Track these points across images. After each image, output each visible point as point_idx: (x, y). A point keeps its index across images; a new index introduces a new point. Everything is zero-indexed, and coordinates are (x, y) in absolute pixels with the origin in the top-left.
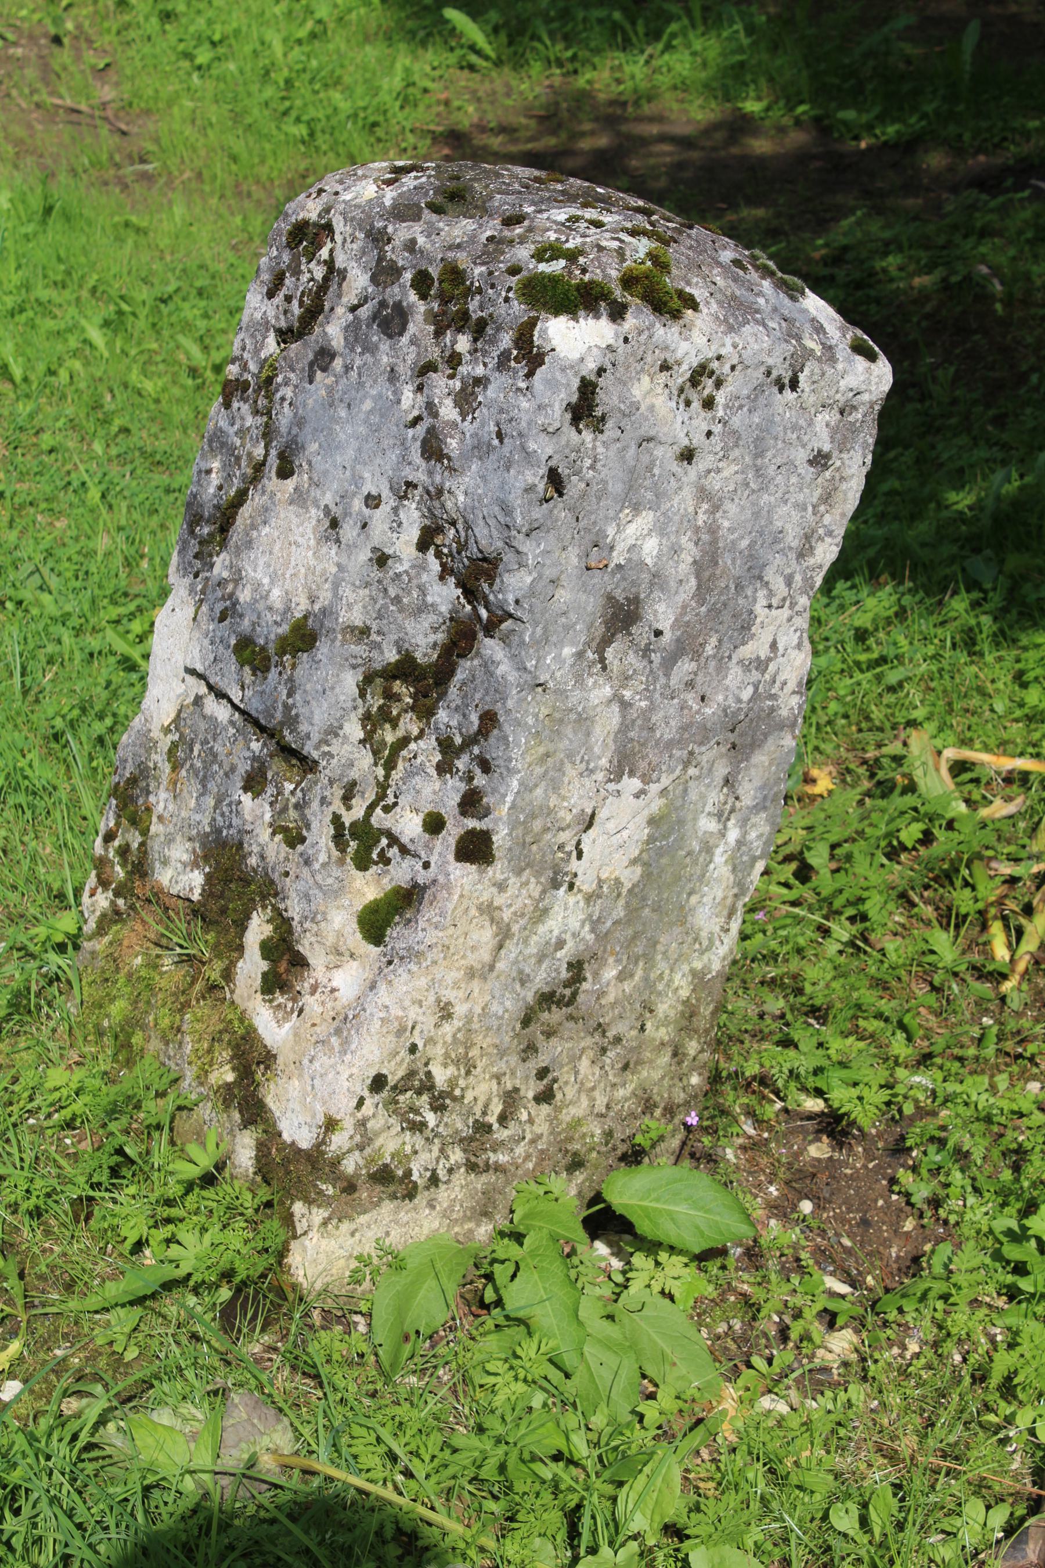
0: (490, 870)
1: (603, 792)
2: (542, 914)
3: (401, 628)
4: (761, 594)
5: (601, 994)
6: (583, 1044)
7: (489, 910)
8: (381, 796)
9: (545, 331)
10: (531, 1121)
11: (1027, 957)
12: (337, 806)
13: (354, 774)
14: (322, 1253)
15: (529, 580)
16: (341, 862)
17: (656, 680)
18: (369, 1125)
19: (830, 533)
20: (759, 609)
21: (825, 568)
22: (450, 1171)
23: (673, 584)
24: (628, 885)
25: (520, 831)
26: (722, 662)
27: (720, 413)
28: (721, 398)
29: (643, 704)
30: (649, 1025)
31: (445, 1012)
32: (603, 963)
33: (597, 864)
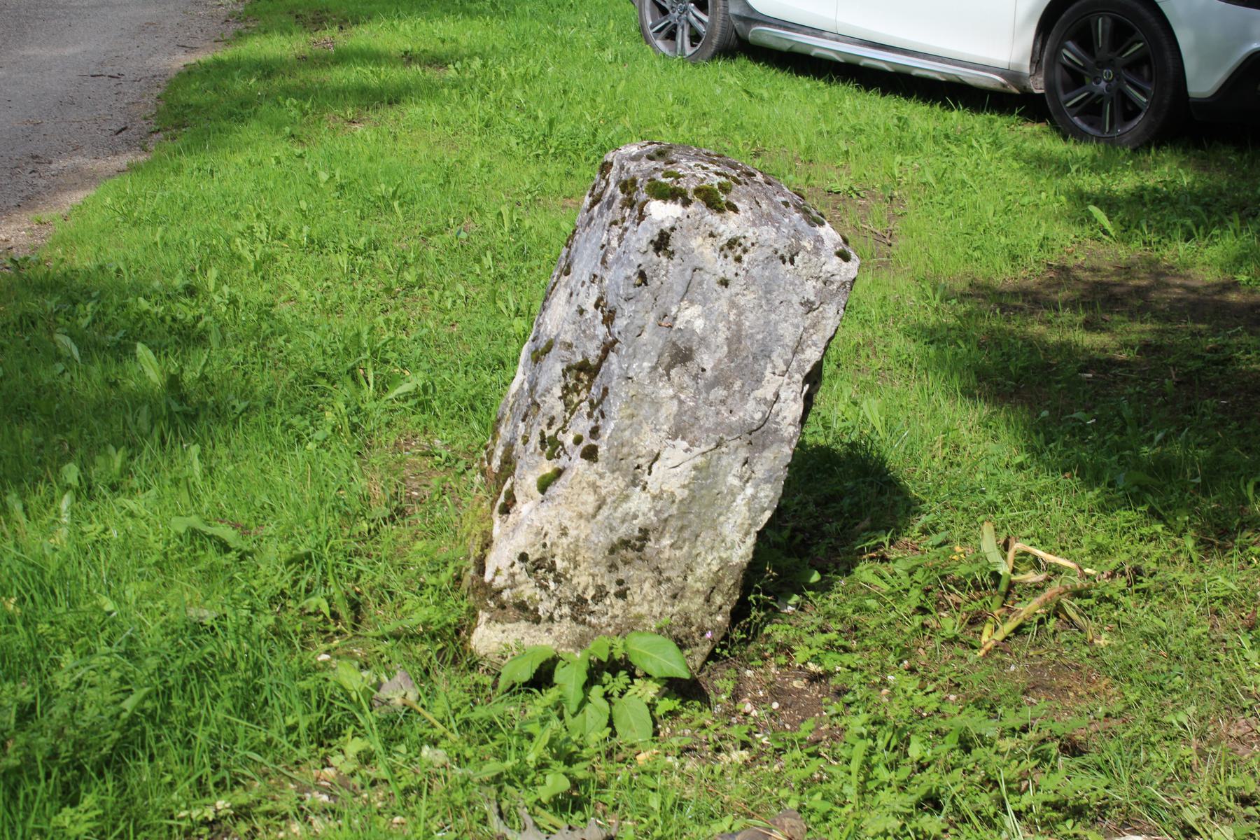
2: (627, 498)
4: (769, 366)
5: (659, 552)
7: (595, 487)
8: (564, 426)
10: (612, 606)
12: (544, 427)
13: (554, 413)
14: (487, 637)
16: (541, 454)
17: (700, 393)
19: (815, 345)
20: (768, 373)
22: (561, 617)
23: (713, 347)
25: (614, 450)
26: (744, 398)
28: (745, 258)
30: (690, 578)
31: (564, 533)
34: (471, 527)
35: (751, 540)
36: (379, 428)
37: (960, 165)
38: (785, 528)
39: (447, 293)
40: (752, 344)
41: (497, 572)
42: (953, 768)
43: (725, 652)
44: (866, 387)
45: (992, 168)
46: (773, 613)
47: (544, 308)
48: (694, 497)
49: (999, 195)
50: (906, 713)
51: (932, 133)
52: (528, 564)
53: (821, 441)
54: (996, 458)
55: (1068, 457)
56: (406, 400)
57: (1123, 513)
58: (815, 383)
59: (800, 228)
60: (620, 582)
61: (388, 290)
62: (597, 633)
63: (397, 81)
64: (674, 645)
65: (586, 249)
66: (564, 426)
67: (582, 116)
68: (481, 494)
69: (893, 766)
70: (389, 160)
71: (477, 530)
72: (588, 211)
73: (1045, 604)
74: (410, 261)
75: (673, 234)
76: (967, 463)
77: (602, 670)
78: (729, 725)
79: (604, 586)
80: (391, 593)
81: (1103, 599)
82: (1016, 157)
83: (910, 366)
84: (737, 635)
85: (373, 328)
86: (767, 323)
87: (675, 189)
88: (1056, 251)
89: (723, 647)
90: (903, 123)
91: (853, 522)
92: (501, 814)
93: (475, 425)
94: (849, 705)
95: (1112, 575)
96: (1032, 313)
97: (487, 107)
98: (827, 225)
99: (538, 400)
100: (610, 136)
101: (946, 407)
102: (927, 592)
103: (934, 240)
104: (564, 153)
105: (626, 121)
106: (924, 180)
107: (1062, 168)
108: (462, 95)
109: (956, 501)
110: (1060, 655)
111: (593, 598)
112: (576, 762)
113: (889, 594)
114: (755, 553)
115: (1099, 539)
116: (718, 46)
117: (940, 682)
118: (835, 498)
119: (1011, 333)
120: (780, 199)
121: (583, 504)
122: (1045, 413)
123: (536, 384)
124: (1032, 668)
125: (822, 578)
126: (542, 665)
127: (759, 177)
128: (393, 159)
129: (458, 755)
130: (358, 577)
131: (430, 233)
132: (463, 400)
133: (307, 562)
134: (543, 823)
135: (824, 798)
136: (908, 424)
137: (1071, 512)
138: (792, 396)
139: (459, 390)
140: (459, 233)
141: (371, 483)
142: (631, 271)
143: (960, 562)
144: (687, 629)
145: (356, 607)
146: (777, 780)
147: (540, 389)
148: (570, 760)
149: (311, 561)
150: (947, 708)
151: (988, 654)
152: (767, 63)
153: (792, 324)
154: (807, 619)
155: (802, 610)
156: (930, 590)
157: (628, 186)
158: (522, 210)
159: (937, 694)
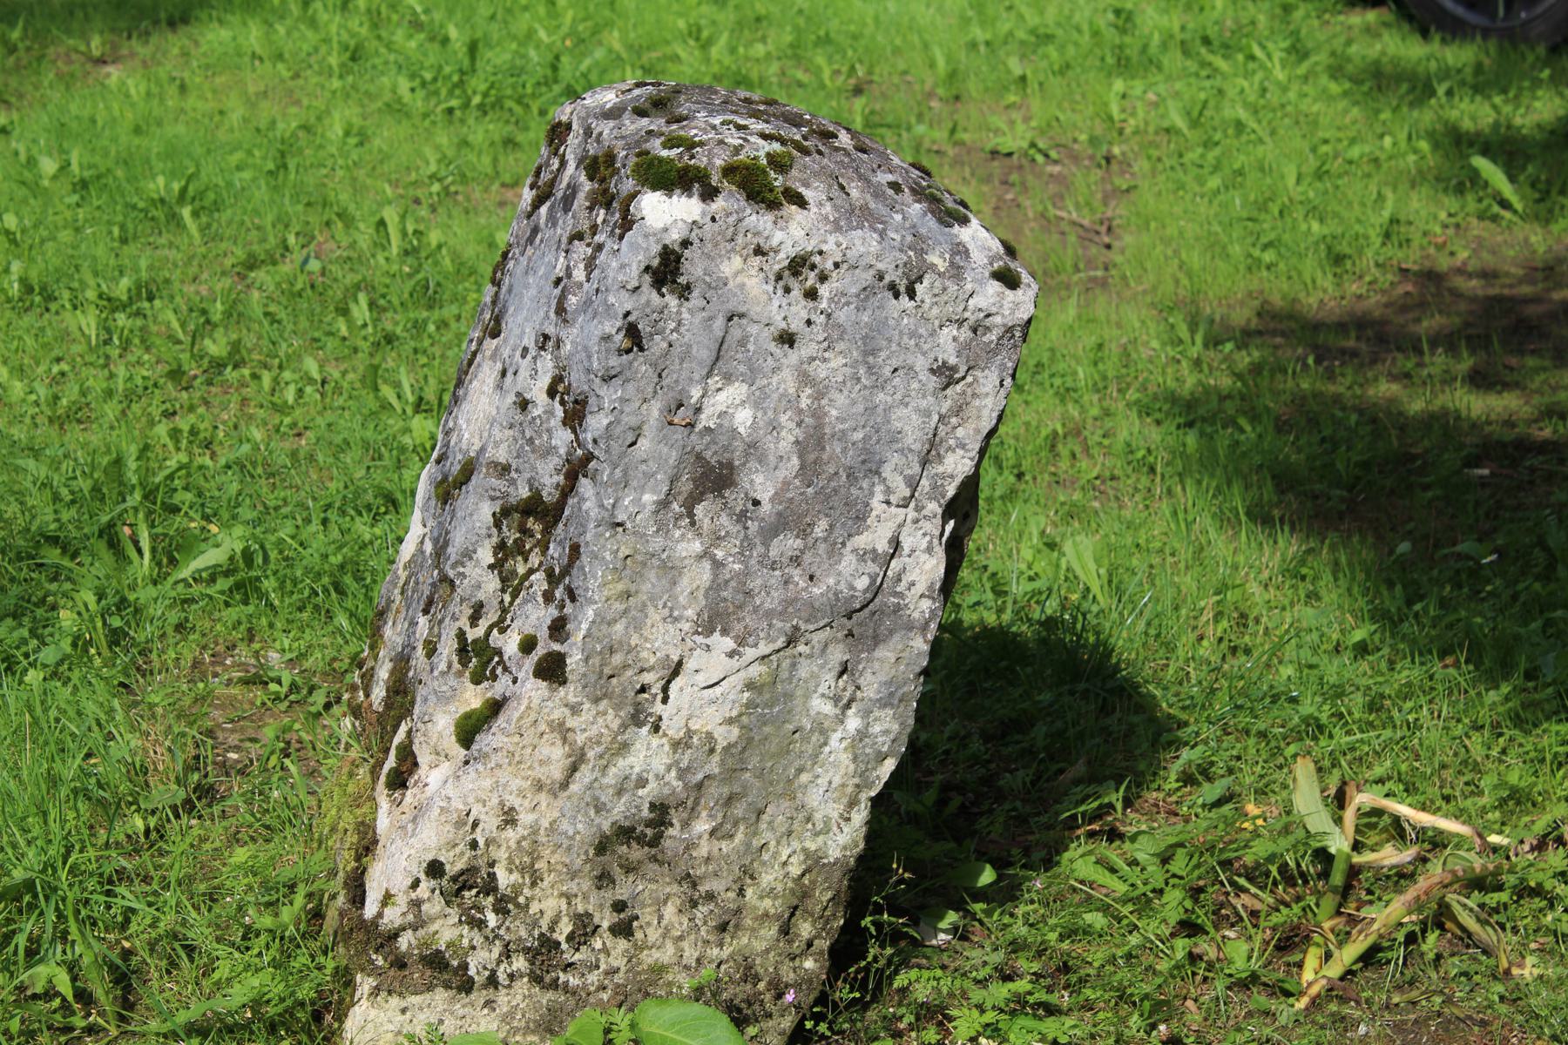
0: (562, 691)
1: (690, 644)
2: (624, 747)
3: (533, 468)
4: (879, 489)
5: (690, 846)
6: (668, 890)
7: (563, 731)
8: (502, 619)
10: (606, 951)
11: (1324, 982)
12: (464, 623)
13: (481, 596)
15: (605, 422)
16: (460, 674)
17: (752, 546)
19: (963, 446)
22: (511, 977)
23: (772, 459)
24: (721, 744)
25: (596, 661)
26: (835, 551)
27: (824, 305)
28: (824, 291)
29: (737, 567)
30: (749, 892)
31: (509, 818)
33: (684, 713)
34: (337, 814)
35: (860, 816)
36: (163, 635)
37: (1232, 93)
38: (929, 785)
39: (287, 375)
40: (844, 450)
41: (387, 898)
43: (823, 1028)
45: (1292, 95)
46: (909, 949)
47: (456, 400)
49: (1305, 146)
51: (1179, 36)
52: (444, 882)
53: (991, 619)
54: (1315, 636)
55: (1450, 626)
56: (212, 580)
57: (1555, 728)
58: (966, 516)
59: (923, 231)
60: (619, 907)
61: (176, 374)
62: (581, 1003)
64: (725, 1019)
65: (527, 286)
66: (502, 619)
67: (530, 34)
68: (353, 754)
70: (170, 130)
71: (348, 820)
72: (529, 216)
73: (1417, 906)
76: (1262, 647)
79: (589, 915)
80: (190, 950)
81: (1525, 891)
82: (1336, 72)
83: (1152, 470)
84: (844, 993)
85: (146, 448)
86: (870, 410)
87: (687, 169)
88: (1415, 244)
89: (819, 1018)
91: (1055, 767)
93: (342, 620)
95: (1540, 846)
96: (1374, 362)
97: (354, 24)
98: (974, 222)
99: (451, 573)
101: (1220, 545)
102: (1196, 892)
104: (498, 104)
105: (614, 39)
106: (1166, 124)
107: (1420, 88)
109: (1244, 719)
110: (1448, 1001)
111: (570, 938)
113: (1126, 900)
114: (869, 838)
115: (1513, 778)
118: (1019, 724)
119: (1337, 399)
120: (884, 178)
121: (542, 763)
122: (1404, 547)
123: (446, 543)
124: (1398, 1027)
127: (844, 139)
128: (181, 129)
130: (127, 921)
131: (252, 264)
132: (319, 575)
133: (27, 898)
137: (1459, 730)
138: (924, 544)
140: (306, 261)
141: (144, 743)
142: (611, 326)
143: (1256, 834)
144: (749, 986)
145: (124, 978)
147: (452, 551)
149: (35, 896)
151: (1315, 1003)
153: (917, 410)
154: (975, 954)
155: (964, 938)
156: (1201, 890)
157: (599, 166)
158: (423, 212)
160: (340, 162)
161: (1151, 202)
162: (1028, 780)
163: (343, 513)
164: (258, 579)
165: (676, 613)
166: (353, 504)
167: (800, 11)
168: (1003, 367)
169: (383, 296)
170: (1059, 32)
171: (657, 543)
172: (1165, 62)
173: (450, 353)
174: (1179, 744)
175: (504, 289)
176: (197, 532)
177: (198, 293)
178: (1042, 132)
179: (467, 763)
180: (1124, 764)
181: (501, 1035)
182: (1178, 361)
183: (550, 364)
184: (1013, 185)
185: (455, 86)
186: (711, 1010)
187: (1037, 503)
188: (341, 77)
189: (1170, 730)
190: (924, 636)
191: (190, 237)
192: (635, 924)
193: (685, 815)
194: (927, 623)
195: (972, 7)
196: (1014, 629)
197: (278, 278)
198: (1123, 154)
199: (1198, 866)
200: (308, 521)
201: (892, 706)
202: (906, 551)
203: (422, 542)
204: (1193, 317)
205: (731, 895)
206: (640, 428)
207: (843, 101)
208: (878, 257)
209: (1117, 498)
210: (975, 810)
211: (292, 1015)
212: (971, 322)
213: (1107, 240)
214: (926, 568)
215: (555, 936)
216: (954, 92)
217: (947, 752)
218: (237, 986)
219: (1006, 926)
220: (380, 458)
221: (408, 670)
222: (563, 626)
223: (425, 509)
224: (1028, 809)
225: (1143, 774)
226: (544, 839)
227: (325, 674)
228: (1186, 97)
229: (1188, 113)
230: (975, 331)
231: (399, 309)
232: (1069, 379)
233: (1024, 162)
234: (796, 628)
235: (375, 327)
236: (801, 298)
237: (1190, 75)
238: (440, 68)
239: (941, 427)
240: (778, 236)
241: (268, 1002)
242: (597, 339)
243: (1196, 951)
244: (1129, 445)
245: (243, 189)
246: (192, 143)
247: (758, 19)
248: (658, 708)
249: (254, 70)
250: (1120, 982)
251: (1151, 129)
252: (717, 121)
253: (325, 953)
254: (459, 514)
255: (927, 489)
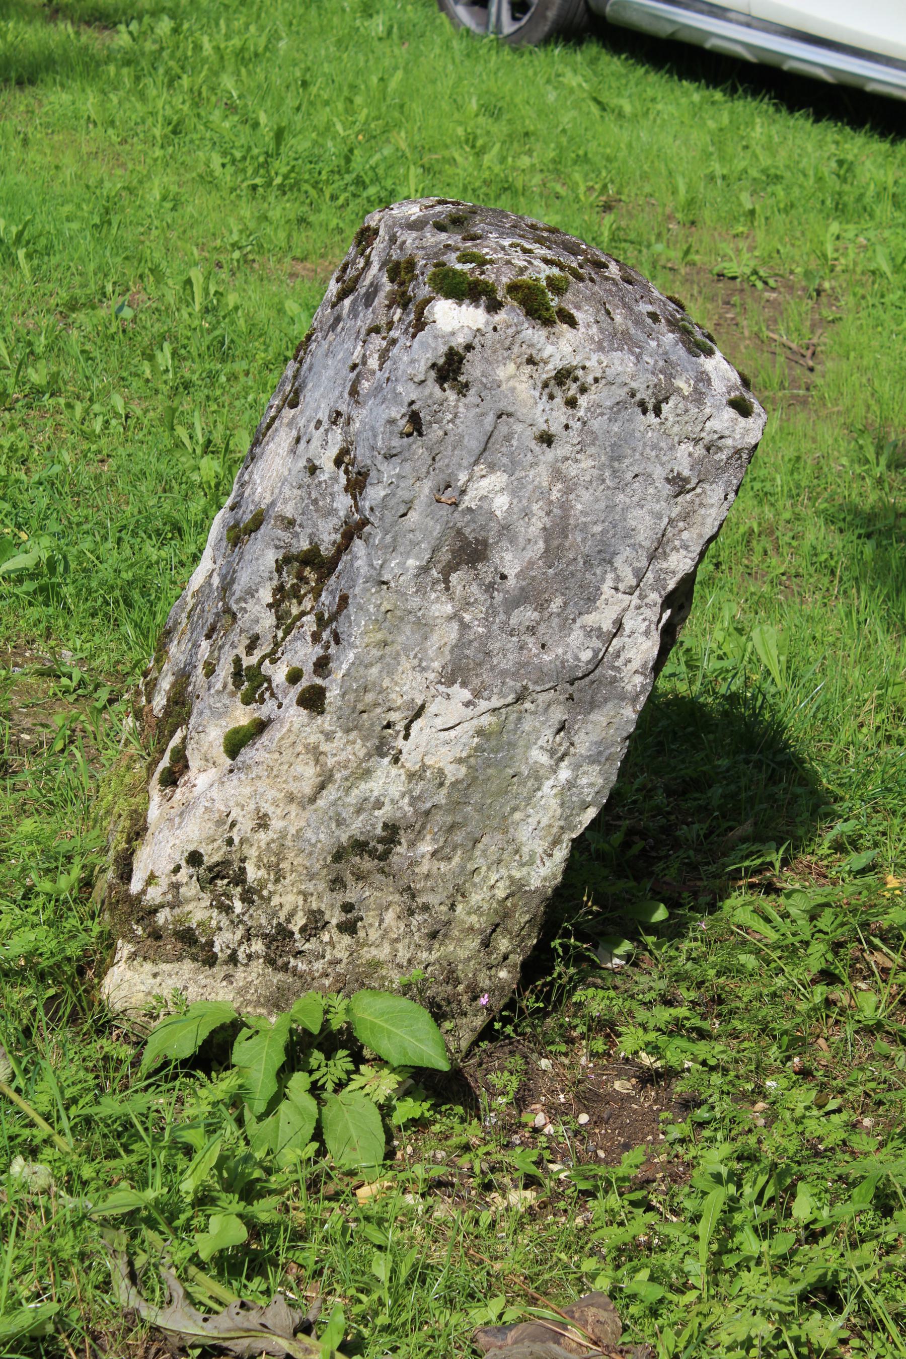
2: (367, 774)
3: (315, 525)
4: (610, 576)
5: (413, 863)
6: (390, 898)
8: (274, 652)
9: (436, 309)
12: (241, 651)
13: (258, 629)
14: (128, 983)
15: (383, 494)
16: (233, 694)
17: (495, 614)
18: (182, 890)
19: (686, 548)
20: (606, 589)
21: (679, 576)
22: (249, 957)
23: (521, 541)
25: (351, 697)
26: (566, 625)
27: (581, 413)
28: (583, 401)
29: (481, 630)
30: (459, 908)
31: (263, 823)
32: (420, 835)
33: (421, 749)
34: (113, 800)
35: (561, 853)
39: (96, 408)
40: (584, 540)
41: (151, 879)
42: (862, 1241)
43: (509, 1029)
44: (759, 604)
46: (588, 970)
48: (475, 779)
50: (792, 1146)
51: (892, 189)
52: (201, 871)
53: (682, 688)
56: (20, 580)
59: (674, 358)
60: (347, 908)
63: (34, 47)
65: (325, 367)
66: (274, 652)
67: (329, 126)
69: (765, 1231)
71: (123, 806)
74: (40, 350)
75: (469, 356)
77: (310, 1046)
78: (508, 1146)
79: (321, 912)
83: (833, 573)
84: (530, 1002)
87: (477, 283)
89: (506, 1021)
90: (845, 169)
92: (132, 1276)
93: (128, 629)
94: (701, 1125)
97: (177, 100)
98: (718, 355)
99: (235, 607)
100: (372, 162)
102: (837, 946)
103: (883, 367)
105: (401, 139)
108: (138, 79)
111: (303, 930)
112: (260, 1196)
114: (566, 872)
116: (556, 23)
117: (850, 1095)
118: (699, 784)
120: (645, 308)
121: (295, 779)
123: (233, 581)
125: (671, 916)
126: (213, 1033)
127: (613, 270)
128: (21, 177)
129: (69, 1174)
131: (73, 306)
132: (112, 588)
134: (201, 1295)
135: (652, 1279)
136: (823, 671)
138: (643, 628)
139: (105, 571)
140: (120, 309)
142: (397, 412)
144: (450, 988)
146: (579, 1244)
148: (250, 1192)
150: (860, 1142)
152: (633, 54)
153: (651, 512)
154: (644, 979)
155: (635, 964)
157: (402, 271)
158: (224, 275)
159: (844, 1116)
160: (156, 223)
161: (853, 333)
162: (702, 833)
163: (135, 534)
164: (59, 585)
165: (424, 664)
166: (143, 527)
167: (564, 131)
168: (728, 483)
169: (184, 347)
170: (788, 175)
171: (415, 602)
172: (878, 213)
173: (237, 403)
174: (832, 816)
175: (305, 366)
176: (10, 537)
177: (25, 325)
178: (764, 261)
179: (231, 771)
180: (785, 828)
181: (236, 1005)
182: (863, 478)
183: (340, 438)
184: (734, 305)
185: (260, 166)
186: (415, 1006)
187: (731, 591)
188: (162, 147)
189: (827, 803)
190: (634, 707)
191: (23, 277)
192: (359, 924)
193: (412, 836)
194: (637, 696)
195: (713, 144)
196: (701, 700)
197: (95, 321)
198: (833, 289)
199: (842, 925)
200: (105, 538)
201: (599, 762)
202: (627, 631)
203: (210, 576)
204: (880, 440)
205: (444, 908)
206: (411, 502)
207: (594, 216)
208: (633, 377)
209: (799, 593)
210: (654, 854)
211: (59, 967)
212: (706, 442)
213: (811, 363)
214: (642, 648)
215: (290, 926)
216: (691, 217)
217: (635, 802)
218: (16, 938)
219: (671, 959)
220: (171, 488)
221: (188, 685)
222: (327, 664)
223: (216, 548)
224: (699, 858)
225: (799, 839)
226: (290, 844)
227: (109, 674)
228: (893, 244)
229: (893, 259)
230: (708, 449)
231: (197, 359)
232: (768, 485)
233: (746, 286)
234: (525, 688)
235: (175, 373)
236: (562, 405)
237: (897, 226)
238: (249, 149)
239: (670, 529)
240: (549, 350)
241: (41, 955)
242: (383, 422)
243: (832, 997)
244: (814, 548)
245: (71, 238)
246: (30, 192)
247: (527, 134)
248: (400, 743)
249: (88, 133)
250: (764, 1018)
251: (859, 270)
252: (506, 243)
253: (93, 918)
254: (247, 557)
255: (651, 581)
